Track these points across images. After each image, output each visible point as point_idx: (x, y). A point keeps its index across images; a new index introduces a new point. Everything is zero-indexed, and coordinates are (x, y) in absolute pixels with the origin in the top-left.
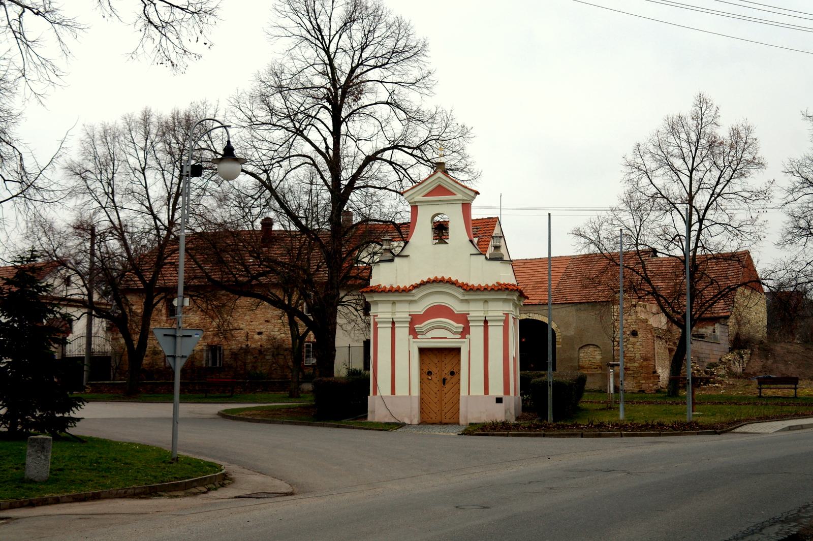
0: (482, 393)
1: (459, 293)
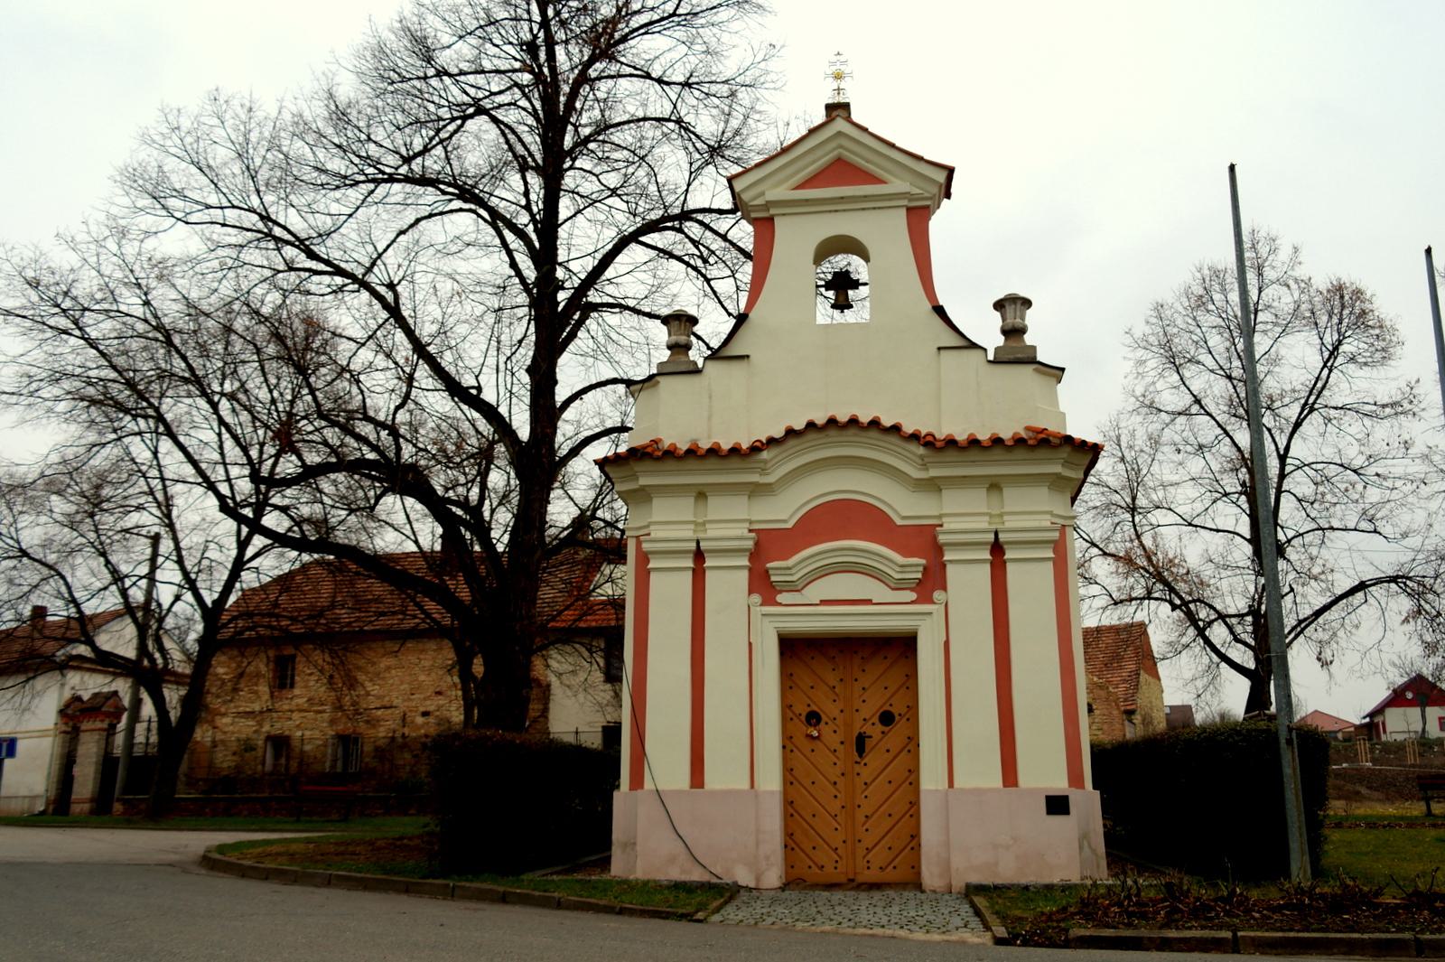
0: (997, 781)
1: (907, 461)
